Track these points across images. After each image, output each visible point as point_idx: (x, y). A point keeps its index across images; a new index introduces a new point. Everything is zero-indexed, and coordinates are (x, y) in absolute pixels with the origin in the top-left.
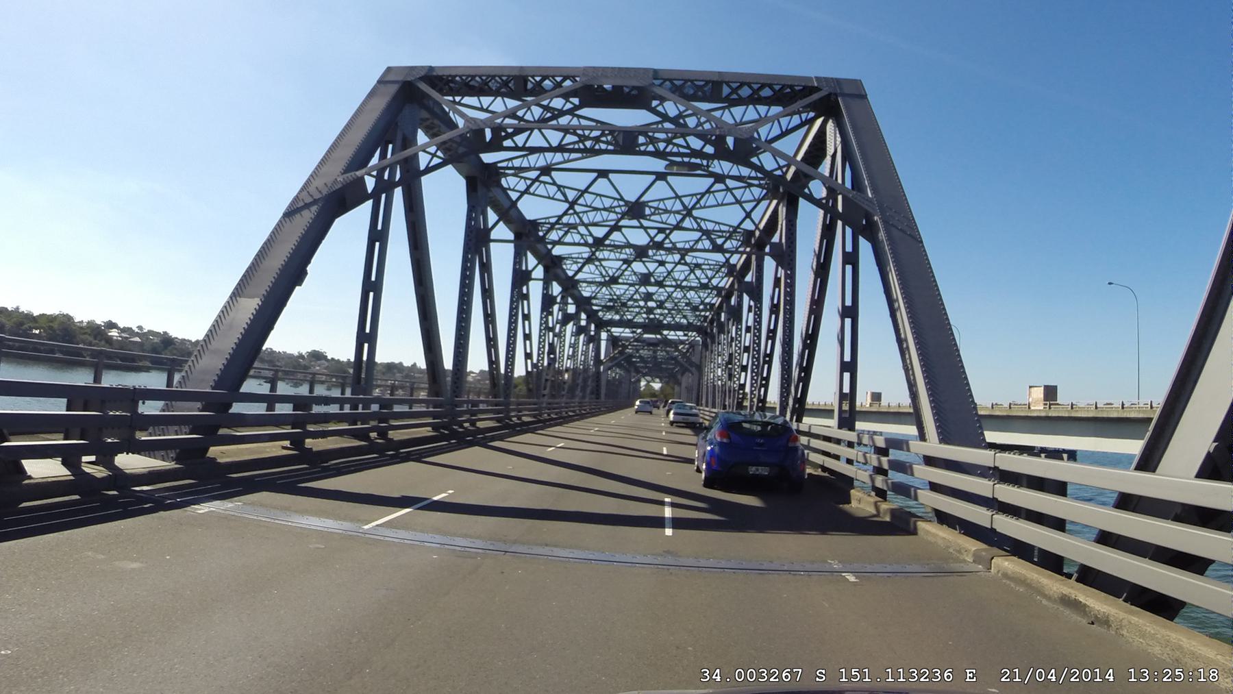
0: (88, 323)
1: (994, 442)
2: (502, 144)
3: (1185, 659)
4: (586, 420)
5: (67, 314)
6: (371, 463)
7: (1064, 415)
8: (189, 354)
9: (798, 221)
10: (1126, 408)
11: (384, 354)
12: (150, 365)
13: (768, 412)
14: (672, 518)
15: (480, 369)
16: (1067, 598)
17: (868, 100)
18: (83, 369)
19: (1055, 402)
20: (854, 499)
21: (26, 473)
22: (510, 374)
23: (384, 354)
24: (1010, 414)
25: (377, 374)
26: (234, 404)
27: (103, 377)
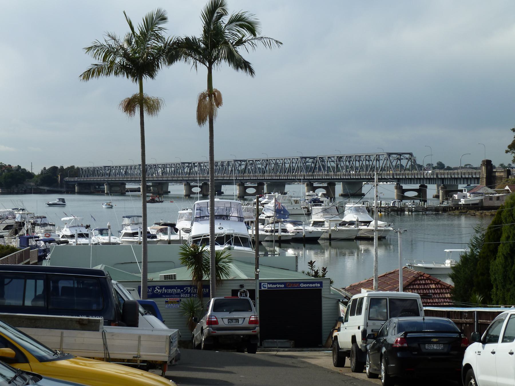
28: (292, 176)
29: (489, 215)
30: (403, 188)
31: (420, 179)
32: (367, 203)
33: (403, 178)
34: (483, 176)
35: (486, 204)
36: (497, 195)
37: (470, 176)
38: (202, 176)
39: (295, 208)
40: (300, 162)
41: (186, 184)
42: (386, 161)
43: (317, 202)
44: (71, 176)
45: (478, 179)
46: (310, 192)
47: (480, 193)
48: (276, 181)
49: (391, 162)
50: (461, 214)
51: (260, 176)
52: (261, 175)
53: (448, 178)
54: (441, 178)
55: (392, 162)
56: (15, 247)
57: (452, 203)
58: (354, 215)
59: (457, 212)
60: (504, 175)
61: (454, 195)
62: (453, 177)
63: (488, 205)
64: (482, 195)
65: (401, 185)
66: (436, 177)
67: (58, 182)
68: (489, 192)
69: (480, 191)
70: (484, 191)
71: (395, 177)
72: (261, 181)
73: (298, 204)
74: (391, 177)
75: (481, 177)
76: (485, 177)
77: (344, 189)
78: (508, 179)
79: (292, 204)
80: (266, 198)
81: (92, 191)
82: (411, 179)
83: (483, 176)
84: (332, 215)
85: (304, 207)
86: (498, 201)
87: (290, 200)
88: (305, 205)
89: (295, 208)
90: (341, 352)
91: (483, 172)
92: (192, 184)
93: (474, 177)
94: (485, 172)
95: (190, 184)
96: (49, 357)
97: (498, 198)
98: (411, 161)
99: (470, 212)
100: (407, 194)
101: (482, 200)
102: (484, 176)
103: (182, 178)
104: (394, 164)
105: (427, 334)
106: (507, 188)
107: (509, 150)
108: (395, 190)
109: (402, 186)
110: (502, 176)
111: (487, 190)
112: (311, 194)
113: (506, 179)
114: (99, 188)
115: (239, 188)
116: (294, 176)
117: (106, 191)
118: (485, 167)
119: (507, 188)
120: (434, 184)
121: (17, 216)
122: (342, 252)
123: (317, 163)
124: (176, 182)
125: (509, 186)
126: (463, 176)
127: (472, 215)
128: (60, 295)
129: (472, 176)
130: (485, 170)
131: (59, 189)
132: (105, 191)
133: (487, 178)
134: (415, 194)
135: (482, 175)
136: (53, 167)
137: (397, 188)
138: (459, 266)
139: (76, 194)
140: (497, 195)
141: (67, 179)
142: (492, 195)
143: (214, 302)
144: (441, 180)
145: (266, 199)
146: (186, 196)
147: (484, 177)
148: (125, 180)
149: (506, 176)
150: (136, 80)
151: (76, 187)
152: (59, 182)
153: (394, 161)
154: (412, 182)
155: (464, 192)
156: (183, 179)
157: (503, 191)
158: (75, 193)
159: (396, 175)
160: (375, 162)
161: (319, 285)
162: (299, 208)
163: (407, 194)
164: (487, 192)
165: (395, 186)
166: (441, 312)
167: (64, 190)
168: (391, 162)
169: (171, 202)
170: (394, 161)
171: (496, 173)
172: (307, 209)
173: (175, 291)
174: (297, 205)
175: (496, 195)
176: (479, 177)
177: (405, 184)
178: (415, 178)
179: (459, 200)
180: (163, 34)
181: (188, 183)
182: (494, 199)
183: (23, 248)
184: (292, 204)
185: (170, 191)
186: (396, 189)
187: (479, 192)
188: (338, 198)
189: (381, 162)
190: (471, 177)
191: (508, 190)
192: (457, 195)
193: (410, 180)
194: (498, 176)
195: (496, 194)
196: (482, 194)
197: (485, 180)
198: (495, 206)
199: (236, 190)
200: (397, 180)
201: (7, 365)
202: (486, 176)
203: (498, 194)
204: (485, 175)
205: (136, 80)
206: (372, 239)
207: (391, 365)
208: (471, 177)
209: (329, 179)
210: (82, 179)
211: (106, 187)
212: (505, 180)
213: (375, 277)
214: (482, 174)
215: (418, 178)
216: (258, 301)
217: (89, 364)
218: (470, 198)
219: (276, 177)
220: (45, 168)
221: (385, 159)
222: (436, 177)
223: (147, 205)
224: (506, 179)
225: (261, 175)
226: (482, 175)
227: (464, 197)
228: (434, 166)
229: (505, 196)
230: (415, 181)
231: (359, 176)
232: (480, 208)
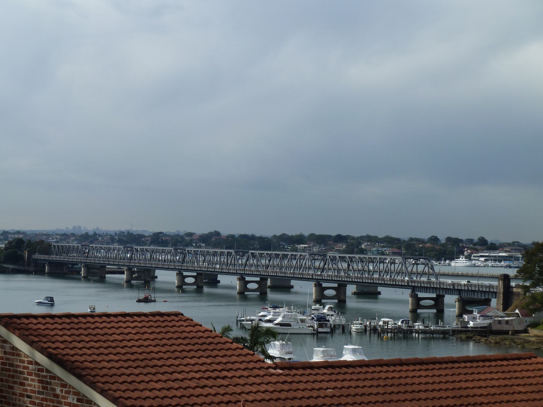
22: (117, 239)
28: (299, 275)
29: (494, 342)
30: (418, 297)
31: (436, 288)
32: (375, 321)
33: (418, 286)
34: (500, 291)
35: (495, 328)
36: (507, 319)
37: (488, 290)
38: (198, 266)
39: (301, 327)
40: (308, 258)
41: (178, 273)
42: (401, 265)
43: (323, 321)
44: (41, 253)
45: (496, 293)
46: (316, 305)
47: (489, 316)
48: (281, 278)
49: (406, 267)
50: (469, 339)
51: (263, 271)
52: (264, 271)
53: (465, 290)
54: (458, 289)
55: (407, 267)
58: (352, 356)
59: (463, 336)
60: (521, 292)
61: (464, 316)
62: (470, 289)
63: (496, 329)
64: (491, 318)
65: (416, 293)
66: (452, 288)
67: (25, 260)
68: (499, 315)
69: (490, 314)
70: (494, 314)
71: (410, 285)
72: (264, 277)
73: (304, 323)
74: (406, 284)
75: (498, 292)
76: (502, 292)
78: (525, 296)
79: (298, 323)
80: (270, 315)
81: (65, 272)
82: (427, 287)
83: (500, 291)
84: (331, 356)
85: (309, 326)
86: (507, 325)
87: (296, 318)
88: (310, 324)
89: (301, 327)
91: (500, 286)
92: (185, 274)
93: (491, 291)
94: (502, 287)
95: (183, 273)
97: (507, 322)
98: (428, 267)
99: (476, 338)
100: (422, 303)
101: (490, 324)
102: (501, 291)
103: (174, 267)
104: (409, 269)
106: (517, 311)
107: (518, 274)
108: (410, 298)
109: (418, 295)
110: (520, 292)
111: (497, 313)
112: (318, 308)
113: (523, 296)
114: (72, 267)
115: (240, 282)
116: (301, 275)
117: (83, 274)
118: (502, 282)
119: (517, 311)
120: (450, 294)
123: (327, 262)
125: (518, 309)
126: (481, 289)
127: (477, 342)
129: (489, 290)
130: (502, 285)
131: (26, 268)
132: (82, 275)
133: (504, 293)
134: (432, 302)
135: (499, 290)
137: (411, 296)
139: (46, 275)
140: (507, 319)
141: (37, 256)
142: (501, 319)
144: (458, 291)
145: (271, 315)
146: (178, 287)
147: (501, 292)
148: (106, 264)
149: (523, 293)
151: (46, 267)
152: (26, 259)
153: (409, 266)
154: (428, 291)
155: (474, 313)
156: (175, 267)
157: (513, 314)
158: (45, 274)
159: (411, 283)
160: (389, 265)
162: (305, 327)
163: (422, 303)
164: (496, 315)
165: (410, 294)
167: (31, 269)
168: (406, 267)
169: (165, 301)
170: (409, 266)
171: (514, 288)
172: (313, 328)
174: (303, 324)
175: (505, 319)
176: (496, 291)
177: (420, 292)
178: (431, 287)
179: (468, 323)
180: (229, 336)
181: (180, 272)
182: (502, 323)
184: (298, 323)
185: (157, 276)
186: (411, 297)
187: (488, 314)
188: (350, 297)
189: (396, 266)
190: (488, 290)
191: (517, 314)
192: (467, 316)
193: (426, 289)
194: (515, 292)
195: (506, 317)
196: (490, 317)
197: (502, 295)
198: (503, 330)
200: (412, 288)
202: (503, 291)
203: (508, 317)
204: (502, 290)
208: (488, 290)
209: (339, 281)
210: (53, 257)
211: (84, 270)
212: (523, 297)
214: (499, 289)
215: (433, 288)
218: (479, 321)
219: (281, 273)
221: (400, 263)
222: (452, 288)
224: (523, 296)
225: (264, 271)
226: (499, 290)
227: (474, 319)
228: (475, 242)
229: (514, 320)
230: (431, 290)
231: (372, 280)
232: (488, 332)
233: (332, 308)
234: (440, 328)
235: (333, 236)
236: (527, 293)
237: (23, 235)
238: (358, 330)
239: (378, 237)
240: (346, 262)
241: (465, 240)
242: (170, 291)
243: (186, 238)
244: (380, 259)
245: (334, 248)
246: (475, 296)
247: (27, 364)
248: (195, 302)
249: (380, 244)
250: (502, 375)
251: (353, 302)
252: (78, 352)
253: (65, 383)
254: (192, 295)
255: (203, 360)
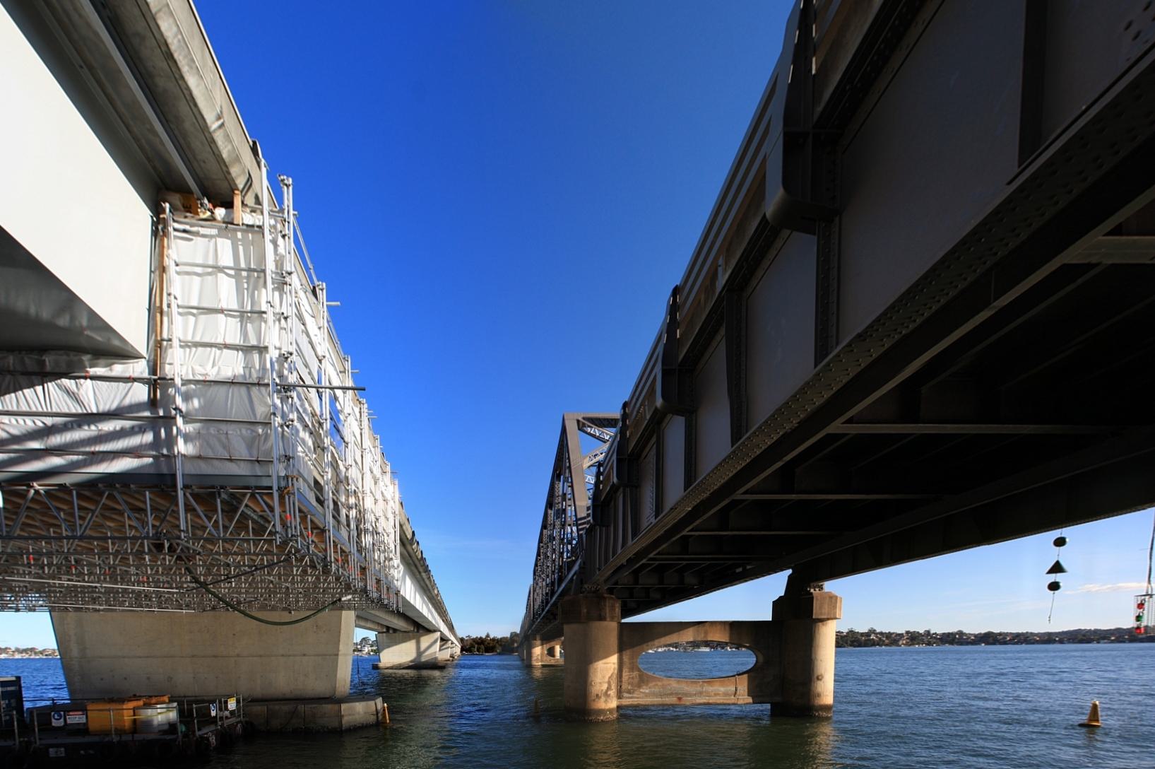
0: (248, 702)
1: (991, 546)
2: (793, 571)
3: (787, 428)
4: (782, 135)
5: (851, 632)
6: (713, 243)
7: (819, 402)
8: (430, 679)
9: (1057, 631)
10: (281, 344)
11: (41, 387)
12: (1073, 255)
13: (716, 715)
14: (621, 650)
15: (961, 629)
16: (325, 729)
17: (183, 482)
18: (591, 674)
19: (5, 689)
20: (1056, 576)
21: (506, 638)
22: (232, 704)
23: (41, 387)
24: (341, 643)
25: (337, 612)
26: (766, 615)
27: (826, 703)
56: (190, 432)
57: (20, 537)
77: (558, 460)
90: (337, 301)
96: (1026, 711)
105: (1031, 167)
121: (191, 543)
122: (312, 413)
124: (170, 282)
128: (623, 621)
136: (989, 544)
138: (428, 697)
143: (813, 651)
150: (809, 737)
161: (178, 562)
166: (840, 665)
167: (690, 579)
173: (327, 458)
183: (53, 492)
199: (177, 363)
201: (612, 449)
205: (809, 737)
206: (155, 374)
207: (664, 546)
213: (711, 716)
216: (733, 262)
217: (1150, 614)
220: (488, 636)
223: (404, 645)
233: (1092, 719)
234: (81, 67)
235: (514, 635)
236: (768, 706)
237: (28, 720)
238: (215, 84)
239: (783, 594)
240: (732, 447)
241: (147, 430)
242: (1090, 726)
243: (734, 649)
244: (25, 577)
245: (557, 519)
246: (269, 485)
247: (242, 511)
248: (878, 317)
249: (245, 281)
250: (1147, 41)
251: (300, 280)
252: (827, 693)
253: (660, 549)
254: (722, 689)
255: (71, 384)
